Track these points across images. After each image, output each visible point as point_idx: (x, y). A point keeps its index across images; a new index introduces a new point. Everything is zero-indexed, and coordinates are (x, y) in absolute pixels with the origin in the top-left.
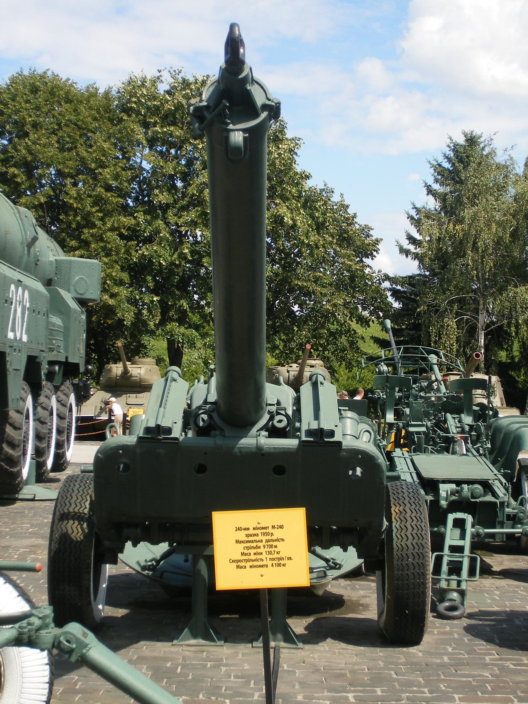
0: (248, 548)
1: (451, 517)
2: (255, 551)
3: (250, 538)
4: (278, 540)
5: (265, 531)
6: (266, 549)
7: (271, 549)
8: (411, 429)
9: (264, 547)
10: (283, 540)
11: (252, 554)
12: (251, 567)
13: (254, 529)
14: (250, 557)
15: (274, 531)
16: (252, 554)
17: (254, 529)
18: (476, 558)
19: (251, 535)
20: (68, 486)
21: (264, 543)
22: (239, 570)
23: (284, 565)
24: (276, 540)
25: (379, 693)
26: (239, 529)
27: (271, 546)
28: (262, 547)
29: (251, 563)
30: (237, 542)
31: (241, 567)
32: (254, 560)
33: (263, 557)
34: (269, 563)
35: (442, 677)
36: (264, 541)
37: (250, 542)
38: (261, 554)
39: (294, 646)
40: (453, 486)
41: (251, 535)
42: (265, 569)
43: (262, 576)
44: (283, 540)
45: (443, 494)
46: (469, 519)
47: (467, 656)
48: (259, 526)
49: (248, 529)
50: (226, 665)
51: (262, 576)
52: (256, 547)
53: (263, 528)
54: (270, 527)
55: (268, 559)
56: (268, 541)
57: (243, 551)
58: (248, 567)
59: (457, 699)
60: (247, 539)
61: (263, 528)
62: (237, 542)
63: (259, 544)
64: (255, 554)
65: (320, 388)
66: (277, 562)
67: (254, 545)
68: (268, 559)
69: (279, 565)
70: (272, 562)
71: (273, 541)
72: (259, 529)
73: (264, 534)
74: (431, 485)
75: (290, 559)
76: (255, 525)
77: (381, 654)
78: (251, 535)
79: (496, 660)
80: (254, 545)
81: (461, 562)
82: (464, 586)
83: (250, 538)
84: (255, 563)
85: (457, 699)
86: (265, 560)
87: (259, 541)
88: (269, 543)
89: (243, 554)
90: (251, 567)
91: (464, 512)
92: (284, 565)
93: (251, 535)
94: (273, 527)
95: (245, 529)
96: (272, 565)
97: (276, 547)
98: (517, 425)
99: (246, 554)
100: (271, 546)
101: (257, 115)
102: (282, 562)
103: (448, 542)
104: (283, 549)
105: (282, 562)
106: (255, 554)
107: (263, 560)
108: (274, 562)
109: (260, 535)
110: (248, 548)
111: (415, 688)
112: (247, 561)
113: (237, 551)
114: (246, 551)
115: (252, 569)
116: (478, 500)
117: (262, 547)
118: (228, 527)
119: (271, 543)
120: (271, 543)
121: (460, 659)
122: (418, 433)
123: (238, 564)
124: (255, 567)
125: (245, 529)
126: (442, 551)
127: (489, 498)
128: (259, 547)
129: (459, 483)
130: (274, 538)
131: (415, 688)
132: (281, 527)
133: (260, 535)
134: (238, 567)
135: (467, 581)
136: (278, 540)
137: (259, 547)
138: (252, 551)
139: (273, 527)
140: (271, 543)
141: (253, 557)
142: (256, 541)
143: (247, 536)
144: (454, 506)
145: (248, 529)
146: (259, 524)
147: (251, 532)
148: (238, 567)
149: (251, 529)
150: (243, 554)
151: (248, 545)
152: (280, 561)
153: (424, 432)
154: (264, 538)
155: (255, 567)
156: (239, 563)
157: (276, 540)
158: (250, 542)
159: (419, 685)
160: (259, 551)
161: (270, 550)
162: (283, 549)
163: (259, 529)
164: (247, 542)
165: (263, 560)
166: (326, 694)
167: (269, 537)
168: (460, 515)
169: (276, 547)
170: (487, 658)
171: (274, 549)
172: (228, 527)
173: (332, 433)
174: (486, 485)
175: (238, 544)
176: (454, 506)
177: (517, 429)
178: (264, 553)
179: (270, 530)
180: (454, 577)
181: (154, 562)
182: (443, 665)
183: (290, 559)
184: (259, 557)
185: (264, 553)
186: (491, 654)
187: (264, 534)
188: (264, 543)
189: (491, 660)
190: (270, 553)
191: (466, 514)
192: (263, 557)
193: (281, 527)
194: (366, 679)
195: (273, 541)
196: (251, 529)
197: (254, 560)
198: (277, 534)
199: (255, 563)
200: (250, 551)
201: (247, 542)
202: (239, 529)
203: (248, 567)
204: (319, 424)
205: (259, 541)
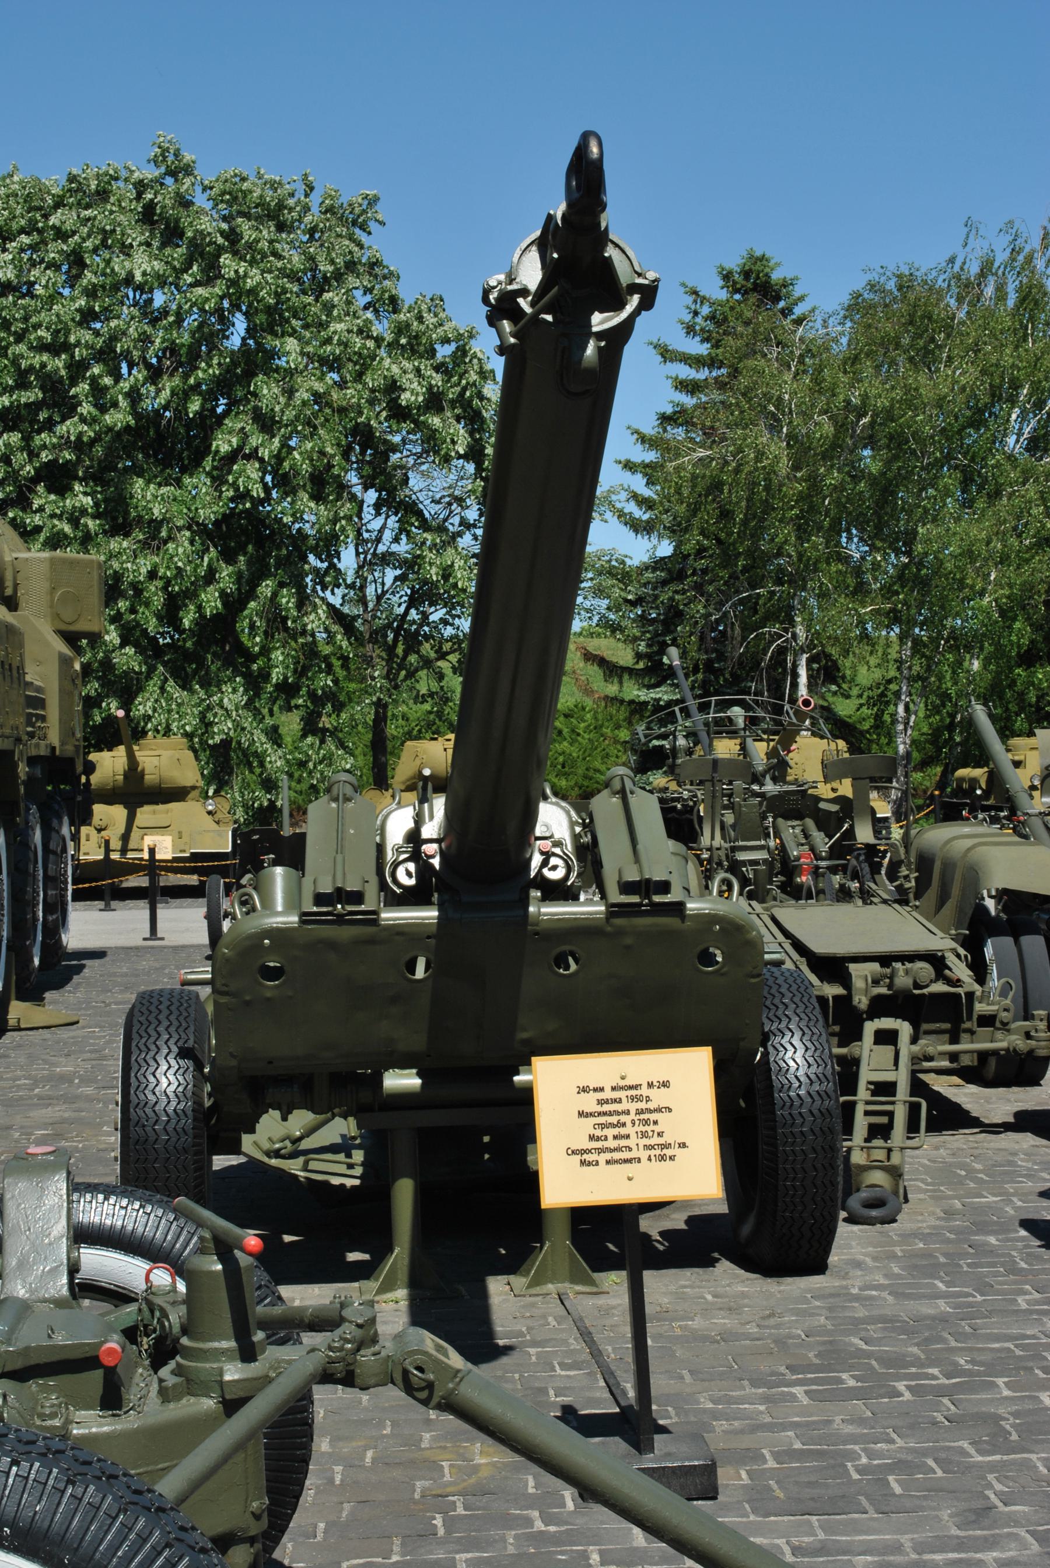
0: (603, 1126)
1: (870, 1028)
2: (616, 1131)
3: (606, 1108)
4: (659, 1110)
5: (634, 1092)
6: (637, 1128)
7: (646, 1128)
8: (742, 856)
9: (633, 1123)
10: (670, 1110)
11: (610, 1138)
12: (608, 1162)
13: (613, 1089)
14: (606, 1144)
15: (653, 1093)
16: (610, 1138)
17: (613, 1089)
18: (919, 1105)
19: (606, 1102)
20: (146, 1012)
21: (632, 1116)
22: (585, 1168)
23: (672, 1158)
24: (656, 1110)
25: (852, 1383)
26: (585, 1090)
27: (646, 1122)
28: (629, 1124)
29: (608, 1156)
30: (581, 1114)
31: (589, 1164)
32: (615, 1150)
33: (631, 1142)
34: (644, 1155)
35: (953, 1344)
36: (633, 1112)
37: (605, 1114)
38: (628, 1137)
39: (595, 1290)
40: (875, 966)
41: (607, 1102)
42: (635, 1165)
43: (630, 1179)
44: (670, 1110)
45: (858, 983)
46: (905, 1029)
47: (979, 1298)
48: (622, 1083)
49: (602, 1089)
50: (535, 1344)
51: (630, 1179)
52: (619, 1127)
53: (631, 1088)
54: (645, 1086)
55: (641, 1147)
56: (639, 1112)
57: (592, 1132)
58: (602, 1162)
59: (1002, 1385)
60: (599, 1109)
61: (631, 1088)
62: (581, 1114)
63: (623, 1118)
64: (615, 1137)
65: (632, 800)
66: (658, 1152)
67: (614, 1119)
68: (641, 1147)
69: (662, 1158)
70: (649, 1152)
71: (650, 1111)
72: (622, 1088)
73: (633, 1099)
74: (832, 967)
75: (683, 1145)
76: (617, 1081)
77: (818, 1303)
78: (606, 1102)
79: (1037, 1302)
80: (614, 1119)
81: (891, 1114)
82: (896, 1159)
83: (606, 1108)
84: (617, 1156)
85: (1002, 1385)
86: (635, 1148)
87: (623, 1112)
88: (642, 1117)
89: (592, 1138)
90: (608, 1162)
91: (896, 1016)
92: (672, 1158)
93: (607, 1102)
94: (650, 1085)
95: (595, 1090)
96: (650, 1159)
97: (656, 1123)
98: (969, 843)
99: (598, 1139)
100: (646, 1122)
101: (620, 306)
102: (668, 1152)
103: (866, 1075)
104: (670, 1127)
105: (668, 1152)
106: (615, 1137)
107: (630, 1149)
108: (653, 1152)
109: (624, 1100)
110: (603, 1126)
111: (914, 1370)
112: (600, 1151)
113: (580, 1133)
114: (598, 1133)
115: (610, 1166)
116: (925, 991)
117: (629, 1124)
118: (560, 1086)
119: (645, 1116)
120: (647, 1116)
121: (970, 1305)
122: (754, 863)
123: (584, 1157)
124: (616, 1162)
125: (595, 1090)
126: (855, 1094)
127: (940, 987)
128: (624, 1125)
129: (885, 960)
130: (651, 1105)
131: (914, 1370)
132: (665, 1084)
133: (624, 1100)
134: (583, 1163)
135: (902, 1149)
136: (659, 1110)
137: (624, 1125)
138: (610, 1132)
139: (650, 1085)
140: (645, 1116)
141: (611, 1143)
142: (618, 1113)
143: (600, 1102)
144: (880, 1007)
145: (602, 1089)
146: (623, 1078)
147: (608, 1094)
148: (583, 1163)
149: (608, 1089)
150: (592, 1138)
151: (602, 1120)
152: (665, 1151)
153: (765, 861)
154: (633, 1107)
155: (616, 1162)
156: (585, 1156)
157: (656, 1110)
158: (605, 1114)
159: (917, 1362)
160: (623, 1131)
161: (644, 1129)
162: (670, 1127)
163: (622, 1088)
164: (599, 1114)
165: (630, 1149)
166: (749, 1390)
167: (642, 1105)
168: (887, 1023)
169: (656, 1123)
170: (1020, 1300)
171: (652, 1127)
172: (560, 1086)
173: (664, 887)
174: (937, 961)
175: (583, 1119)
176: (880, 1007)
177: (969, 850)
178: (633, 1136)
179: (644, 1091)
180: (878, 1142)
181: (287, 1143)
182: (943, 1319)
183: (683, 1145)
184: (623, 1143)
185: (633, 1136)
186: (1026, 1293)
187: (633, 1099)
188: (632, 1116)
189: (1028, 1302)
190: (644, 1135)
191: (899, 1021)
192: (631, 1142)
193: (665, 1084)
194: (811, 1355)
195: (650, 1111)
196: (608, 1089)
197: (615, 1150)
198: (659, 1098)
199: (617, 1156)
200: (606, 1132)
201: (599, 1114)
202: (585, 1090)
203: (602, 1162)
204: (641, 872)
205: (623, 1112)
